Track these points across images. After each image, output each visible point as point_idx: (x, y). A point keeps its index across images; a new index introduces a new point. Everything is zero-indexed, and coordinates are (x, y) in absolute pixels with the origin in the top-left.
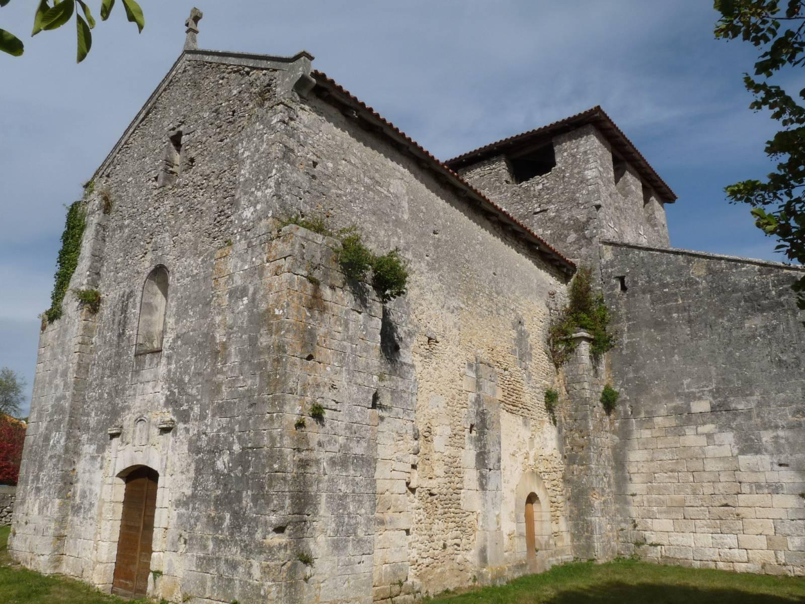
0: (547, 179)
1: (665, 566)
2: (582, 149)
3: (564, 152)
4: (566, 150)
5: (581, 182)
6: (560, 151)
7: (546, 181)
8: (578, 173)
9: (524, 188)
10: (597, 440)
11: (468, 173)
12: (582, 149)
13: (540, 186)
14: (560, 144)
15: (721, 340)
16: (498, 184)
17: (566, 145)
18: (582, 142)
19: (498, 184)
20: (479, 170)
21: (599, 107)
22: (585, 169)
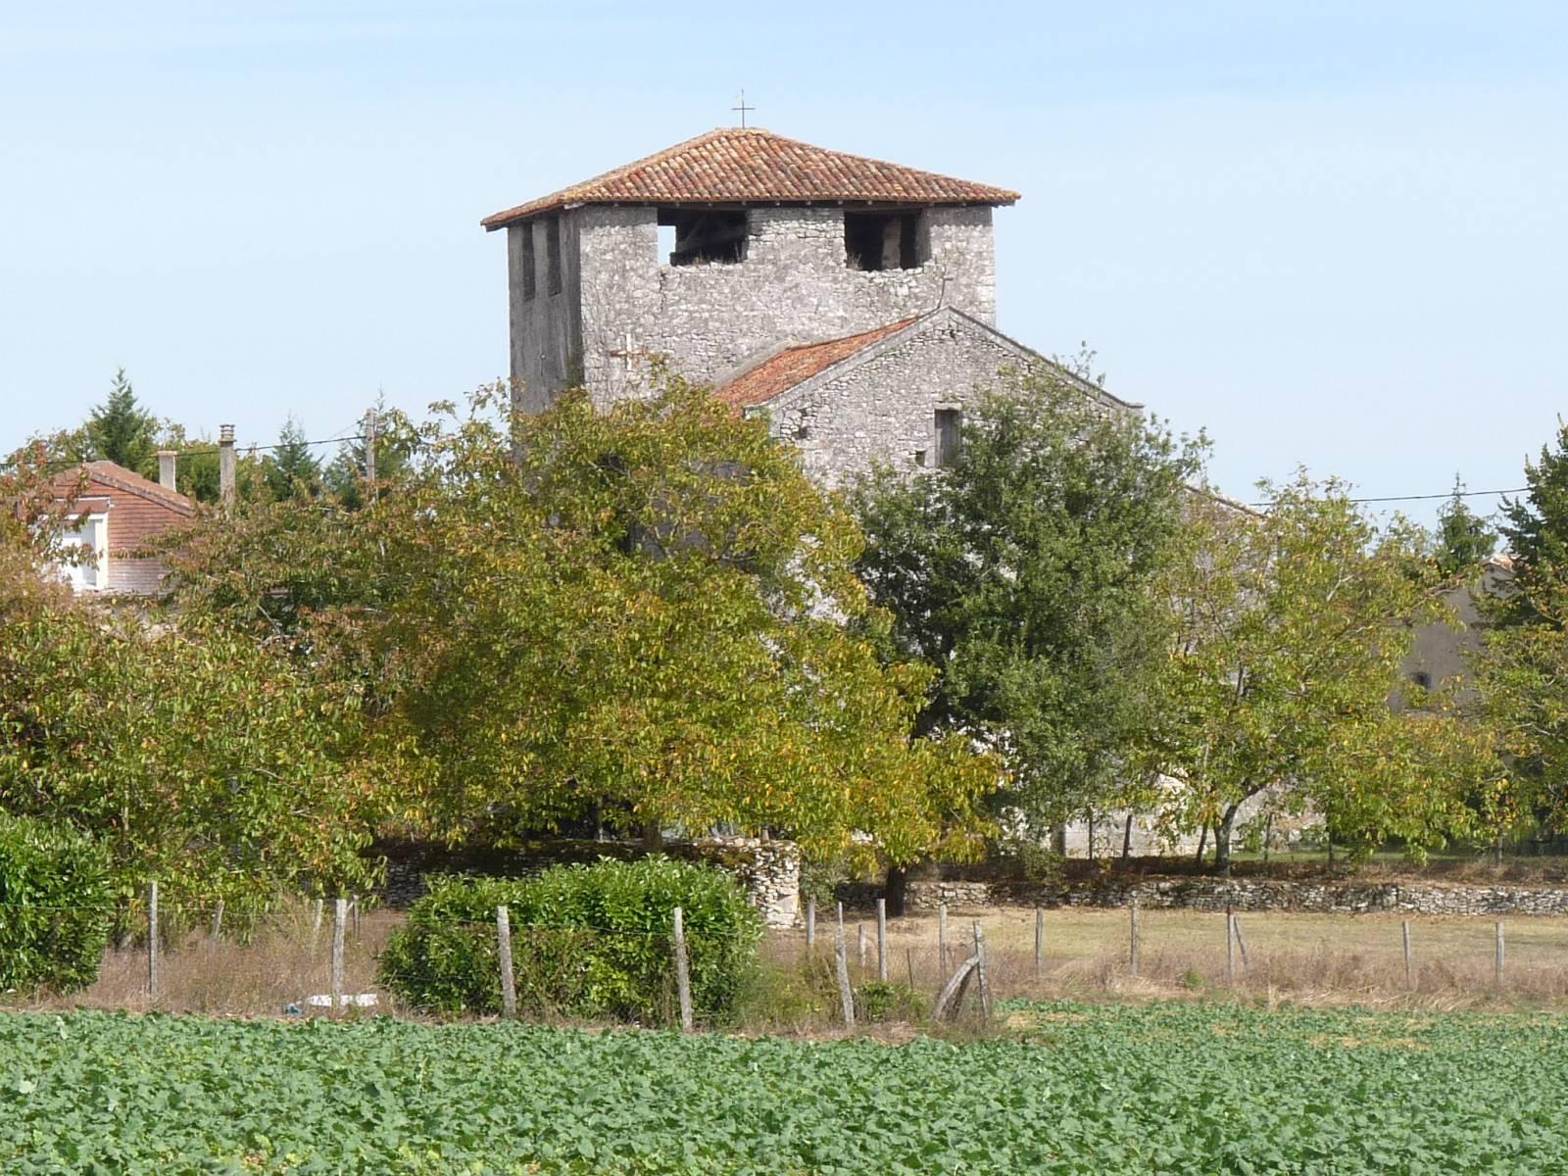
0: (917, 280)
1: (628, 806)
2: (975, 247)
3: (776, 236)
4: (949, 239)
5: (971, 303)
6: (939, 236)
7: (913, 284)
8: (968, 286)
9: (877, 285)
10: (419, 470)
11: (772, 223)
12: (975, 247)
13: (904, 291)
14: (941, 225)
15: (514, 488)
16: (832, 263)
17: (950, 230)
18: (976, 234)
19: (832, 263)
20: (795, 224)
21: (520, 224)
22: (978, 283)
